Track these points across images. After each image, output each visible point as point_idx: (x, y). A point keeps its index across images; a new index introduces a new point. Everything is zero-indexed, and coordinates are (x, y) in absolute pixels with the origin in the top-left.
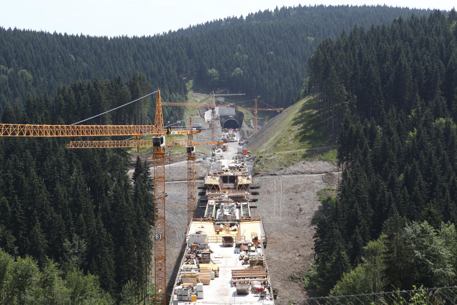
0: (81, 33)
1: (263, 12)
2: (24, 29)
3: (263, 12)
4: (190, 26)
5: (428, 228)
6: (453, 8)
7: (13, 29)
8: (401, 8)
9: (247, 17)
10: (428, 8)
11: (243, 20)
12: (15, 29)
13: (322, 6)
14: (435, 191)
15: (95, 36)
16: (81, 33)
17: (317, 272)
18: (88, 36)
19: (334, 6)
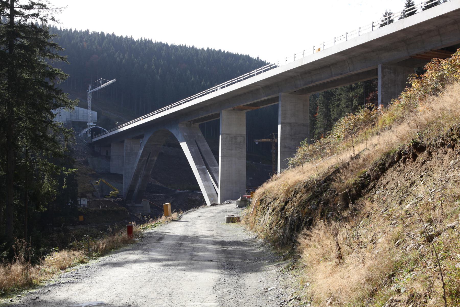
0: (76, 29)
1: (205, 50)
2: (185, 45)
3: (205, 50)
4: (172, 44)
5: (24, 75)
6: (81, 30)
7: (226, 52)
8: (244, 55)
9: (125, 37)
10: (202, 48)
11: (61, 30)
12: (228, 52)
13: (248, 57)
14: (34, 54)
15: (113, 35)
16: (76, 29)
17: (299, 249)
18: (208, 49)
19: (244, 55)
